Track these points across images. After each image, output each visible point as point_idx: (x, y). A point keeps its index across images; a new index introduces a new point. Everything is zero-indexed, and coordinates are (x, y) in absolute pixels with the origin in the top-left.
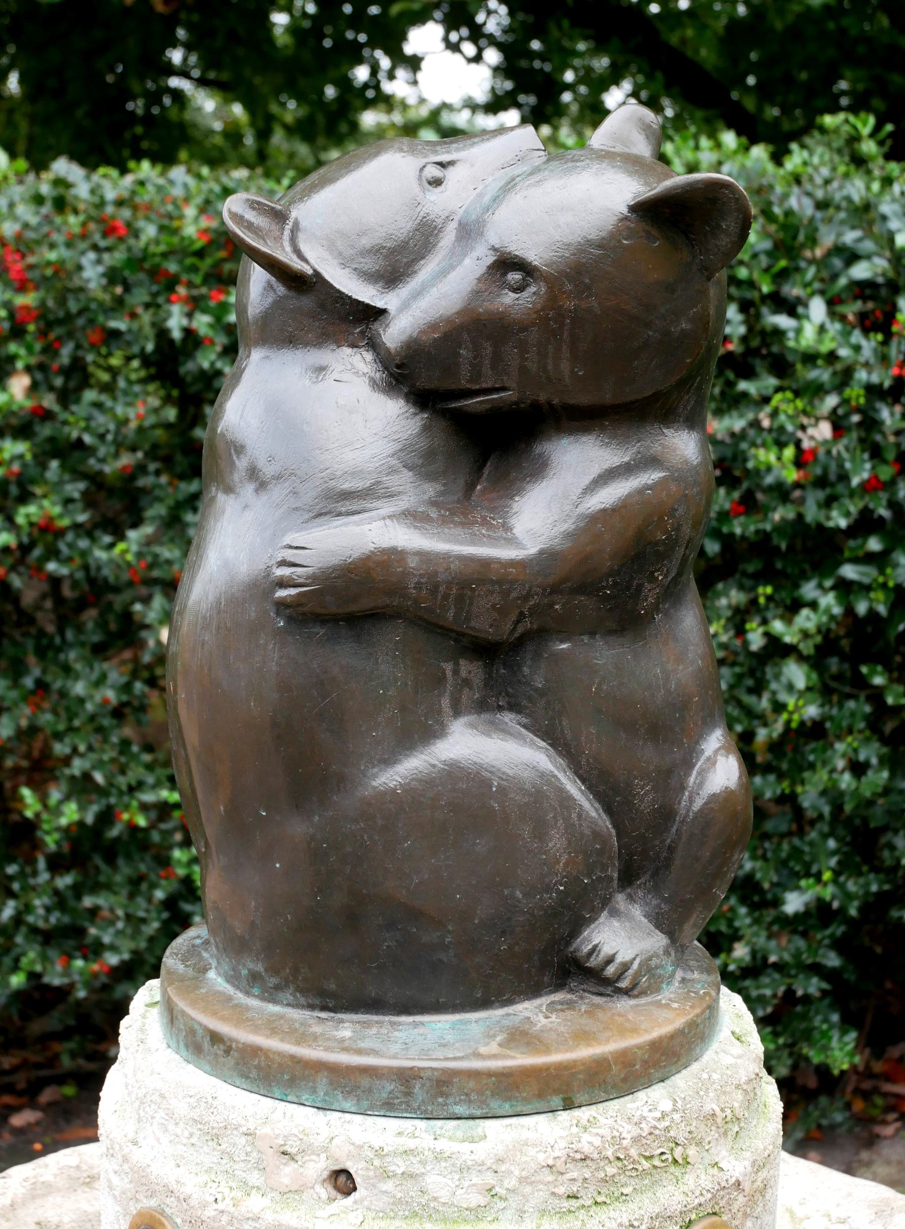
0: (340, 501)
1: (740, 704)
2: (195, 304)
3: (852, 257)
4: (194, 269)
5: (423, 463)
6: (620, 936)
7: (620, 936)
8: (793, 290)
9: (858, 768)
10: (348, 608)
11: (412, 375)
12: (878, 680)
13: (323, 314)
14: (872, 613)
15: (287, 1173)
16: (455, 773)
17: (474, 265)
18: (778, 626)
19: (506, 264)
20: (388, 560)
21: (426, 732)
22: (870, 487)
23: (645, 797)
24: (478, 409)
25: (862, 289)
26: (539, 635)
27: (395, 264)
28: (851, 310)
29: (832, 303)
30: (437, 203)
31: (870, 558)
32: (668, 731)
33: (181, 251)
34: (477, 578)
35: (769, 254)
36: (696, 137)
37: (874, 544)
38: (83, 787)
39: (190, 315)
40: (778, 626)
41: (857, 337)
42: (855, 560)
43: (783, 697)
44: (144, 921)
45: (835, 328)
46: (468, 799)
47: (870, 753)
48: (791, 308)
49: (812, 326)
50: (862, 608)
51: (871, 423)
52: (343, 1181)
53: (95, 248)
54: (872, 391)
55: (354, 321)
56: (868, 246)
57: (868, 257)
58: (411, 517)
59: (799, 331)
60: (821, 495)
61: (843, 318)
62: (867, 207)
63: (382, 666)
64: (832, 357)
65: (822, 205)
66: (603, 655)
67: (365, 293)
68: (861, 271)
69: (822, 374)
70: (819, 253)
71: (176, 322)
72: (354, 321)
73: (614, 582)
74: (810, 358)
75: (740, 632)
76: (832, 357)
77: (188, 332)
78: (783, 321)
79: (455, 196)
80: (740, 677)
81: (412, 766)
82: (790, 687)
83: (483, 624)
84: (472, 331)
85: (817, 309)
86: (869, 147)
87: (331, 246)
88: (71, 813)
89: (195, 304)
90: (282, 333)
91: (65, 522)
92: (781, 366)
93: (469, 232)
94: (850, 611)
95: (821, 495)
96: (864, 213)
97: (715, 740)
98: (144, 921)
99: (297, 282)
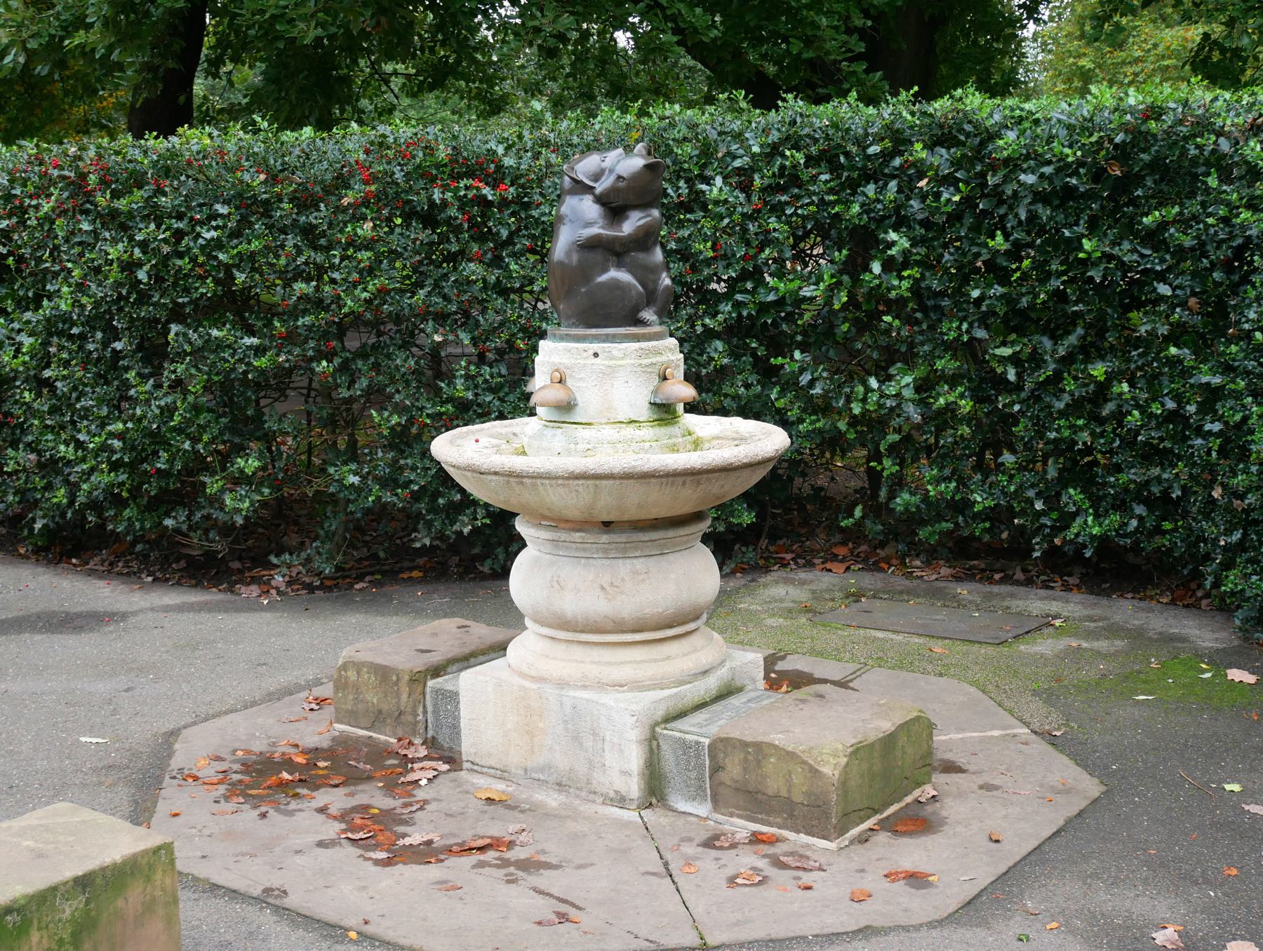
0: (589, 224)
1: (694, 360)
2: (445, 188)
3: (734, 157)
4: (444, 172)
5: (605, 217)
6: (648, 315)
7: (648, 315)
8: (708, 173)
9: (747, 386)
10: (591, 245)
11: (600, 200)
12: (754, 345)
13: (580, 188)
14: (749, 314)
15: (585, 354)
16: (612, 279)
17: (612, 178)
18: (707, 321)
19: (619, 177)
20: (598, 236)
21: (605, 270)
22: (745, 258)
23: (651, 286)
24: (614, 207)
25: (739, 171)
26: (629, 251)
27: (597, 177)
28: (734, 180)
29: (725, 178)
30: (604, 165)
31: (746, 291)
32: (654, 271)
33: (438, 166)
34: (616, 238)
35: (697, 156)
36: (663, 103)
37: (749, 285)
38: (400, 409)
39: (443, 193)
40: (707, 321)
41: (737, 193)
42: (740, 292)
43: (713, 354)
44: (429, 469)
45: (726, 189)
46: (616, 285)
47: (753, 379)
48: (708, 181)
49: (716, 189)
50: (745, 313)
51: (745, 230)
52: (596, 355)
53: (399, 164)
54: (743, 215)
55: (589, 189)
56: (741, 152)
57: (741, 157)
58: (602, 227)
59: (711, 191)
60: (724, 263)
61: (731, 185)
62: (741, 134)
63: (597, 256)
64: (726, 201)
65: (720, 134)
66: (641, 256)
67: (591, 184)
68: (737, 163)
69: (721, 209)
70: (720, 155)
71: (437, 196)
72: (589, 189)
73: (644, 240)
74: (716, 203)
75: (693, 326)
76: (726, 201)
77: (442, 200)
78: (704, 187)
79: (608, 163)
80: (693, 347)
81: (603, 278)
82: (716, 350)
83: (618, 248)
84: (613, 190)
85: (719, 181)
86: (743, 105)
87: (584, 174)
88: (395, 419)
89: (445, 188)
90: (572, 192)
91: (391, 287)
92: (704, 207)
93: (611, 171)
94: (740, 315)
95: (724, 263)
96: (738, 136)
97: (664, 275)
98: (429, 469)
99: (576, 181)
